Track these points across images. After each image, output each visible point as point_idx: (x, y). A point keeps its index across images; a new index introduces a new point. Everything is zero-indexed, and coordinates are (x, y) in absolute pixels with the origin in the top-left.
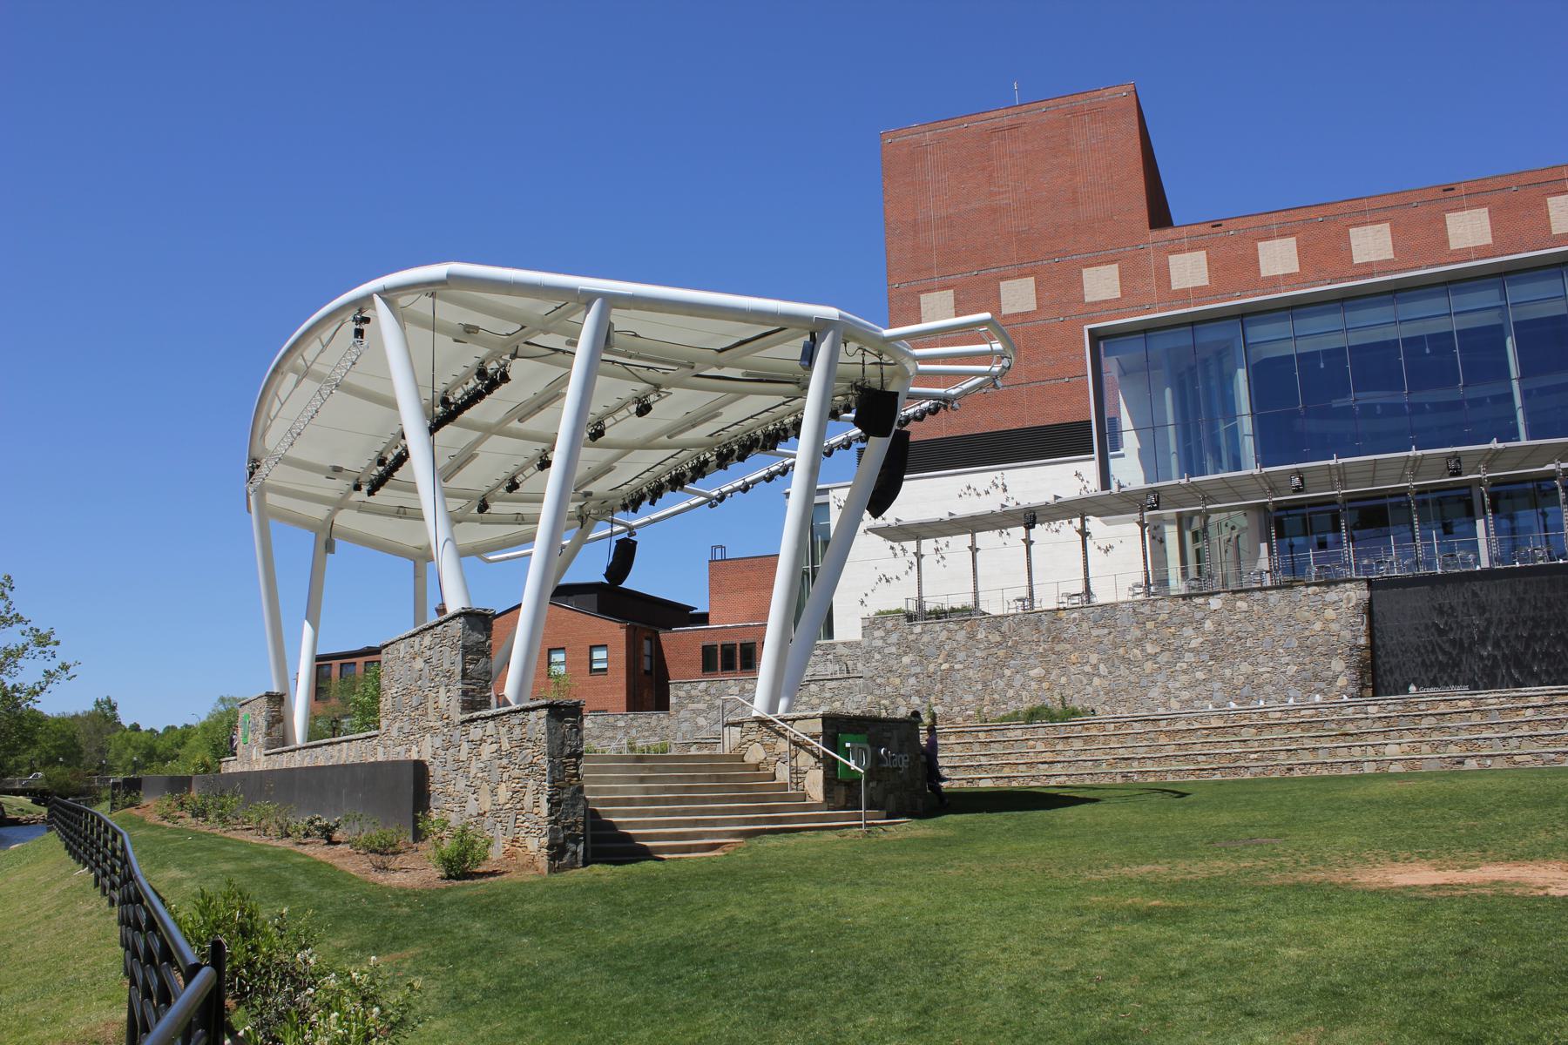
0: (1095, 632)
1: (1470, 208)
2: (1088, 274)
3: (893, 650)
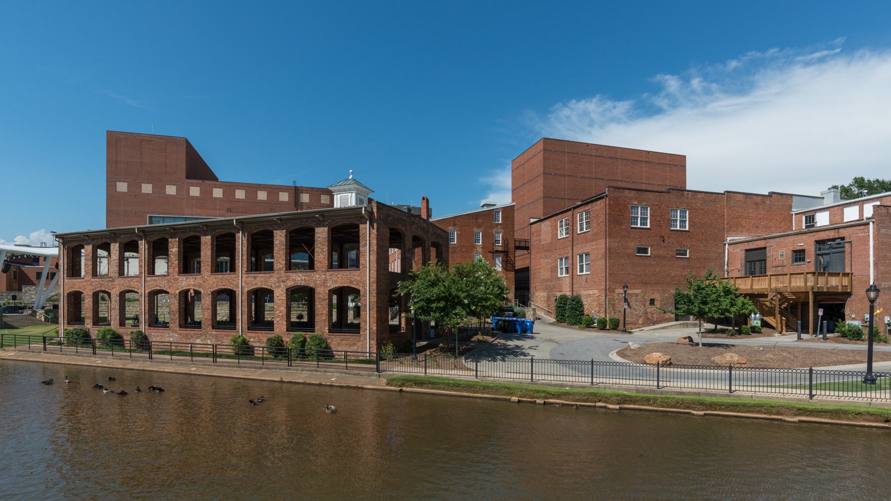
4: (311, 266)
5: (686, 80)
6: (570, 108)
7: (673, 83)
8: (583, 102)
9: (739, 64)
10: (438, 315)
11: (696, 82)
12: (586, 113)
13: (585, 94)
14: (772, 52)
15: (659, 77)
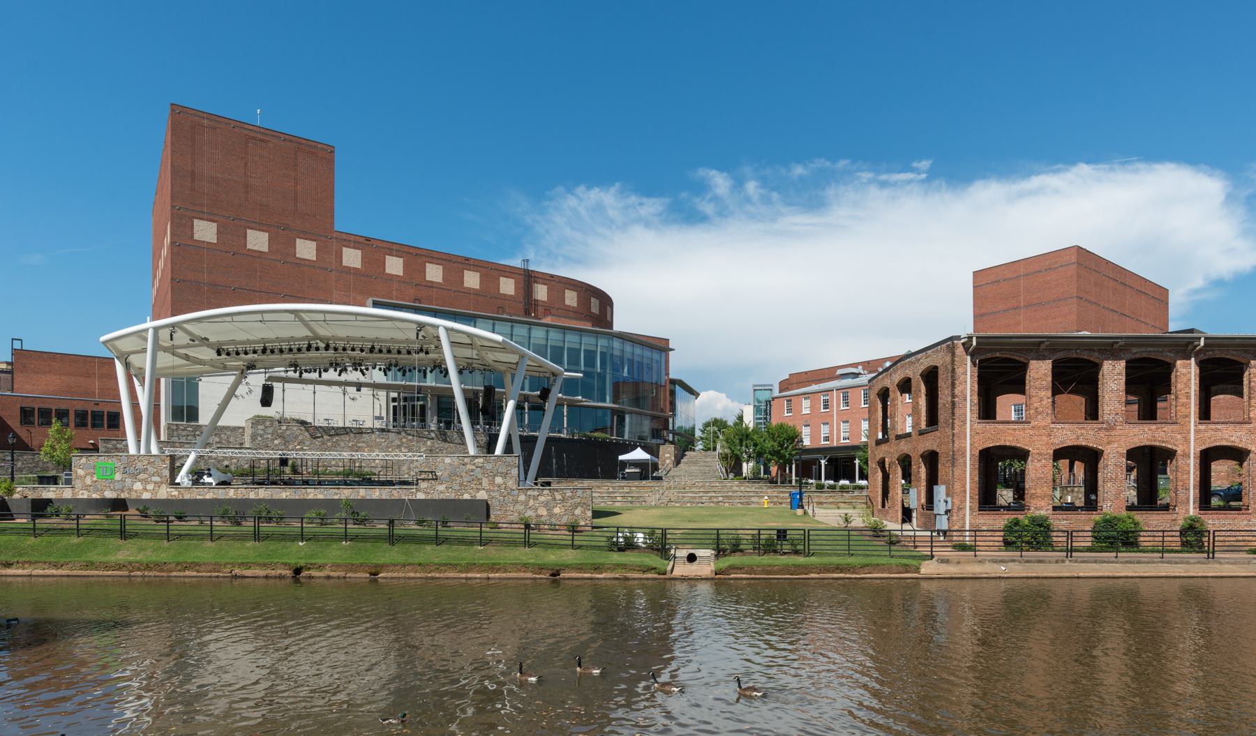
4: (1092, 413)
5: (739, 183)
6: (577, 197)
7: (720, 182)
8: (597, 189)
9: (805, 172)
10: (1039, 491)
11: (751, 187)
12: (599, 208)
13: (599, 178)
14: (842, 164)
15: (701, 172)
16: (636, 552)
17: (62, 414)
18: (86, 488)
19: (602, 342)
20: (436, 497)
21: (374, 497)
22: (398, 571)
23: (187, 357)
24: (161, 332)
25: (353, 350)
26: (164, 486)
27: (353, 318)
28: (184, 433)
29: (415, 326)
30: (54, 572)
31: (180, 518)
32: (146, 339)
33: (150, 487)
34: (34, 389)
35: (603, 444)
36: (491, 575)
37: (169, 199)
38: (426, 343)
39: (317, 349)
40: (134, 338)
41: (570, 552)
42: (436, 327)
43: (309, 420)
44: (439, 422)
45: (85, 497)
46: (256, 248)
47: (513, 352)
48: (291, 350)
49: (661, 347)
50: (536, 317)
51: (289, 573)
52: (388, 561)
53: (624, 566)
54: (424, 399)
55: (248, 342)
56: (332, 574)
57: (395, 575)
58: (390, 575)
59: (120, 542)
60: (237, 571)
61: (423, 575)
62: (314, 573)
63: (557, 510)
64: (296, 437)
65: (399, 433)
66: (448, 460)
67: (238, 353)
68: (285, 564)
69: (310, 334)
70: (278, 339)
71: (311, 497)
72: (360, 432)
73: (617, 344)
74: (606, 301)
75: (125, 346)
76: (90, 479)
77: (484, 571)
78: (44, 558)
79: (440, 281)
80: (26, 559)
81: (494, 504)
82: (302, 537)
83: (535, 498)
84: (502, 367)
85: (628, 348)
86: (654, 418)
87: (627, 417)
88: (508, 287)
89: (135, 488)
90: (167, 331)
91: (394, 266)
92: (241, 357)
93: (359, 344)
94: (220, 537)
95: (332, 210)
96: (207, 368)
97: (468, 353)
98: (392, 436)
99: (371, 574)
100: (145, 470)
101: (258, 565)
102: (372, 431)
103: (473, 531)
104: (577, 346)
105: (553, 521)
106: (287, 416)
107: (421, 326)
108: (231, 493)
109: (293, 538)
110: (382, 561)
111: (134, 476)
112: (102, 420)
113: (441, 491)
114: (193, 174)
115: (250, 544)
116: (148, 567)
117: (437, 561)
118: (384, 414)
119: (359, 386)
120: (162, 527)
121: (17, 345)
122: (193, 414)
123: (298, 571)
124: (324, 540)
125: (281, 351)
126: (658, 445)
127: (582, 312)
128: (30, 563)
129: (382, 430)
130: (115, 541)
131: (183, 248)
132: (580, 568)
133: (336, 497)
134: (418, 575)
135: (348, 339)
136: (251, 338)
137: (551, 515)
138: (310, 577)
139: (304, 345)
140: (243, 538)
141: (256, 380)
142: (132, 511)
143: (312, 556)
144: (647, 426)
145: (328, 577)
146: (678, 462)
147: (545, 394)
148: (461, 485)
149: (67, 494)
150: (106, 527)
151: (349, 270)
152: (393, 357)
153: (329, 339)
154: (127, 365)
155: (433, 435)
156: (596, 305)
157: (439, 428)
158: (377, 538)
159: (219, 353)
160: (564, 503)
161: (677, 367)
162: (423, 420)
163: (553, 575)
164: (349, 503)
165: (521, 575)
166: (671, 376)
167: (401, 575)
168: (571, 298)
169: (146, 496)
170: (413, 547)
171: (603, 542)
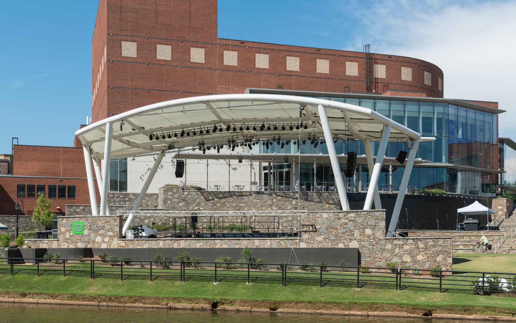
0: (255, 201)
1: (324, 59)
2: (319, 71)
3: (176, 200)
16: (501, 296)
17: (41, 188)
18: (66, 240)
19: (439, 109)
20: (315, 246)
21: (266, 246)
22: (292, 307)
23: (128, 143)
24: (114, 125)
25: (248, 129)
26: (115, 239)
27: (250, 103)
28: (118, 200)
29: (298, 106)
30: (51, 301)
31: (127, 263)
32: (104, 132)
33: (106, 239)
34: (24, 172)
35: (441, 199)
36: (371, 313)
37: (105, 29)
38: (307, 118)
39: (221, 130)
40: (96, 131)
41: (438, 294)
42: (316, 105)
43: (204, 186)
44: (301, 184)
45: (66, 247)
46: (163, 58)
47: (379, 123)
48: (201, 132)
49: (491, 110)
50: (377, 92)
51: (208, 306)
52: (283, 299)
53: (493, 309)
54: (289, 166)
55: (171, 128)
56: (241, 308)
57: (290, 310)
58: (286, 310)
59: (91, 280)
60: (171, 304)
61: (313, 311)
62: (227, 307)
63: (420, 257)
64: (195, 200)
65: (270, 195)
66: (325, 216)
67: (164, 137)
68: (206, 299)
69: (216, 119)
70: (193, 125)
71: (218, 246)
72: (241, 194)
73: (452, 110)
74: (436, 73)
75: (89, 137)
76: (70, 234)
77: (364, 309)
78: (45, 291)
79: (298, 69)
80: (34, 291)
81: (364, 252)
82: (216, 278)
83: (401, 247)
84: (363, 136)
85: (462, 112)
86: (484, 174)
87: (459, 175)
88: (352, 69)
89: (97, 240)
90: (118, 124)
91: (262, 61)
92: (164, 140)
93: (251, 124)
94: (157, 277)
95: (216, 23)
96: (141, 150)
97: (341, 126)
98: (265, 197)
99: (271, 309)
100: (103, 228)
101: (186, 299)
102: (250, 193)
103: (351, 274)
104: (416, 115)
105: (417, 266)
106: (188, 184)
107: (304, 105)
108: (160, 244)
109: (209, 279)
110: (278, 299)
111: (96, 231)
112: (55, 192)
113: (319, 241)
114: (121, 7)
115: (178, 283)
116: (110, 299)
117: (323, 299)
118: (257, 180)
119: (240, 159)
120: (117, 270)
121: (15, 142)
122: (123, 186)
123: (215, 305)
124: (232, 281)
125: (195, 134)
126: (491, 199)
127: (417, 85)
128: (37, 294)
129: (258, 193)
130: (88, 280)
131: (116, 63)
132: (450, 309)
133: (237, 247)
134: (309, 311)
135: (244, 120)
136: (173, 125)
137: (415, 262)
138: (225, 310)
139: (211, 127)
140: (172, 278)
141: (169, 158)
142: (96, 257)
143: (224, 294)
144: (478, 181)
145: (238, 311)
146: (510, 214)
147: (402, 157)
148: (336, 236)
149: (54, 245)
150: (81, 269)
151: (229, 68)
152: (273, 134)
153: (230, 122)
154: (91, 151)
155: (297, 195)
156: (429, 76)
157: (301, 189)
158: (272, 280)
159: (151, 138)
160: (422, 250)
161: (506, 127)
162: (288, 184)
163: (425, 314)
164: (248, 251)
165: (397, 314)
166: (500, 136)
167: (295, 310)
168: (406, 74)
169: (104, 246)
170: (302, 288)
171: (468, 286)
